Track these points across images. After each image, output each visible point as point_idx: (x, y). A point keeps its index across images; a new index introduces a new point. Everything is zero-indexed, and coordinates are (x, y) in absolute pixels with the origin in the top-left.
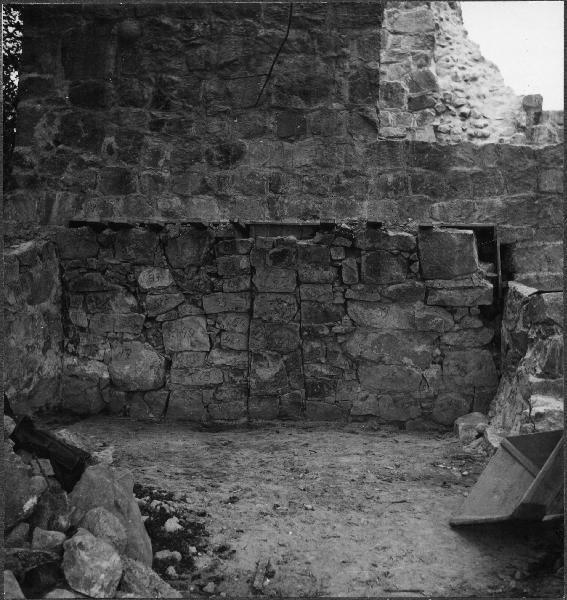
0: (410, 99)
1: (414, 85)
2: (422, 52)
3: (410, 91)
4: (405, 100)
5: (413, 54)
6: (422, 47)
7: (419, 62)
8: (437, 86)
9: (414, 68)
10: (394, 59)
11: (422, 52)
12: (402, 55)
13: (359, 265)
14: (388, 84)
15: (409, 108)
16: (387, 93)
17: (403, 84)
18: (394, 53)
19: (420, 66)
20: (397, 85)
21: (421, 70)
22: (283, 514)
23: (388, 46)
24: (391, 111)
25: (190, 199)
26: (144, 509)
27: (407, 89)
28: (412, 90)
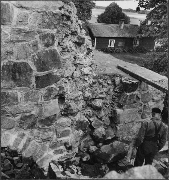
0: (37, 78)
1: (42, 65)
2: (48, 31)
3: (38, 71)
4: (33, 80)
5: (39, 32)
6: (48, 26)
7: (46, 41)
8: (90, 14)
9: (41, 47)
10: (21, 38)
11: (48, 31)
12: (28, 33)
13: (110, 45)
14: (16, 64)
15: (37, 86)
16: (15, 73)
17: (31, 63)
18: (19, 31)
19: (47, 45)
20: (26, 65)
21: (47, 49)
22: (76, 81)
23: (14, 23)
24: (19, 90)
25: (133, 169)
26: (14, 169)
27: (34, 68)
28: (39, 70)
